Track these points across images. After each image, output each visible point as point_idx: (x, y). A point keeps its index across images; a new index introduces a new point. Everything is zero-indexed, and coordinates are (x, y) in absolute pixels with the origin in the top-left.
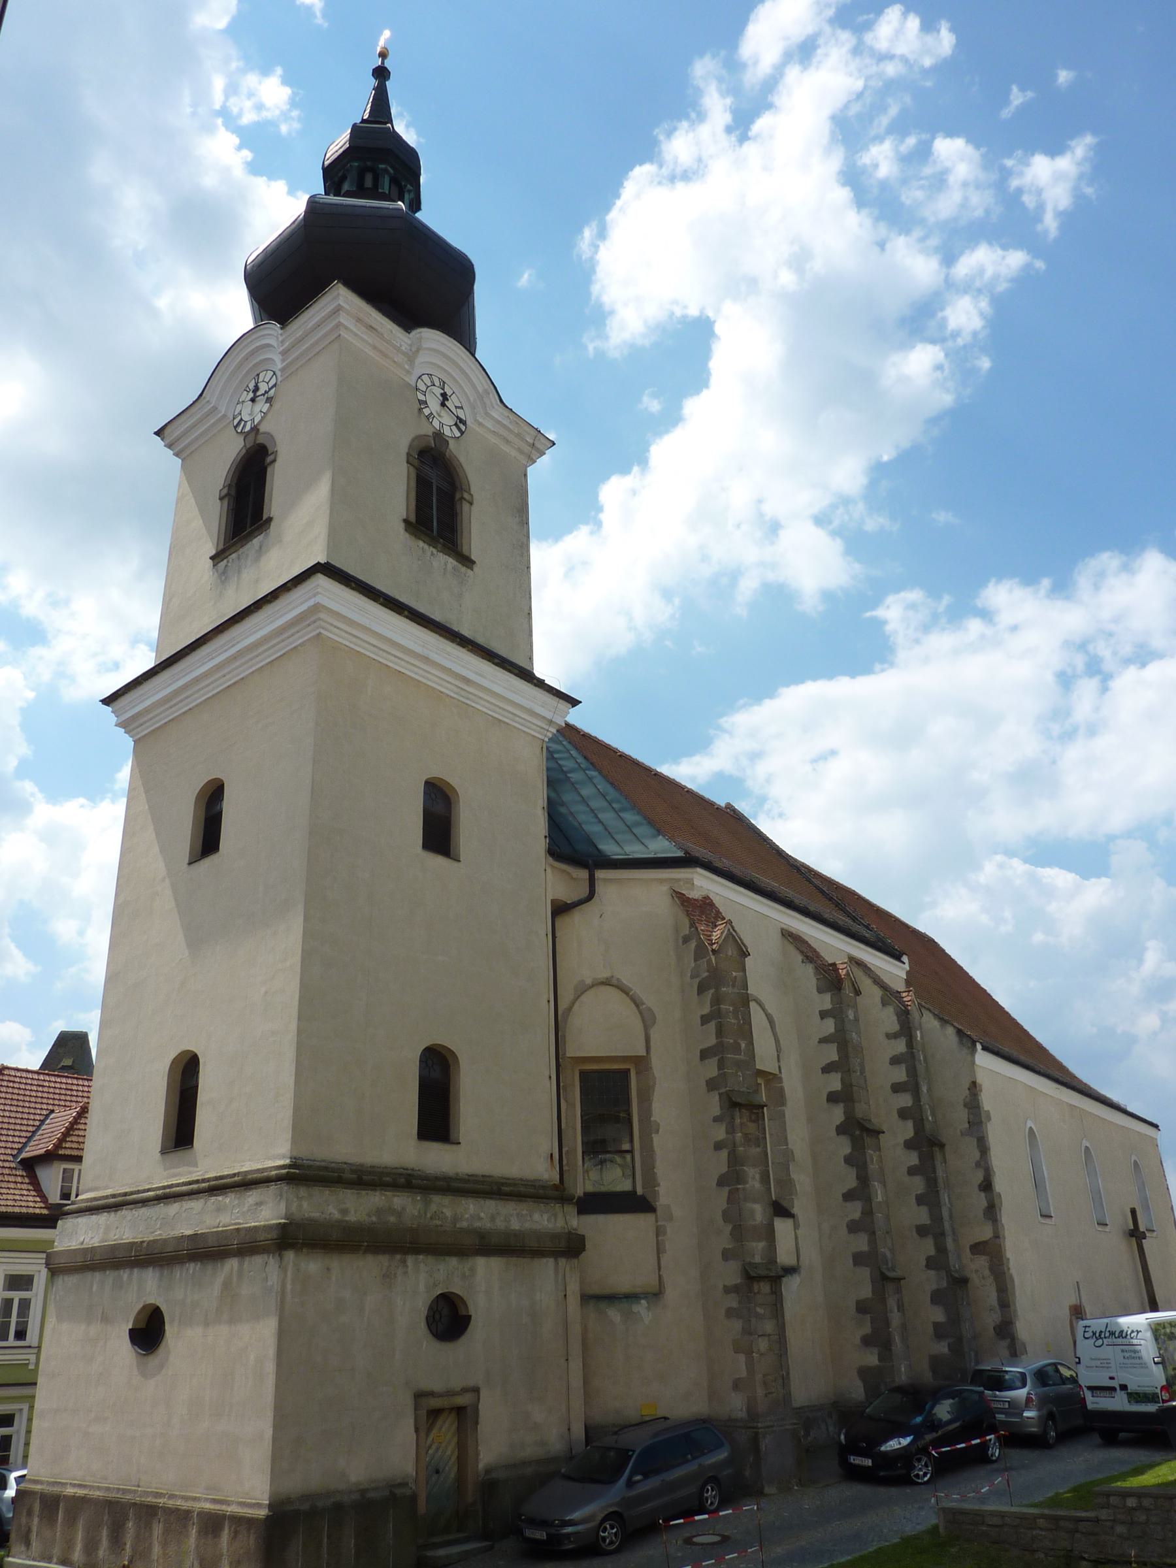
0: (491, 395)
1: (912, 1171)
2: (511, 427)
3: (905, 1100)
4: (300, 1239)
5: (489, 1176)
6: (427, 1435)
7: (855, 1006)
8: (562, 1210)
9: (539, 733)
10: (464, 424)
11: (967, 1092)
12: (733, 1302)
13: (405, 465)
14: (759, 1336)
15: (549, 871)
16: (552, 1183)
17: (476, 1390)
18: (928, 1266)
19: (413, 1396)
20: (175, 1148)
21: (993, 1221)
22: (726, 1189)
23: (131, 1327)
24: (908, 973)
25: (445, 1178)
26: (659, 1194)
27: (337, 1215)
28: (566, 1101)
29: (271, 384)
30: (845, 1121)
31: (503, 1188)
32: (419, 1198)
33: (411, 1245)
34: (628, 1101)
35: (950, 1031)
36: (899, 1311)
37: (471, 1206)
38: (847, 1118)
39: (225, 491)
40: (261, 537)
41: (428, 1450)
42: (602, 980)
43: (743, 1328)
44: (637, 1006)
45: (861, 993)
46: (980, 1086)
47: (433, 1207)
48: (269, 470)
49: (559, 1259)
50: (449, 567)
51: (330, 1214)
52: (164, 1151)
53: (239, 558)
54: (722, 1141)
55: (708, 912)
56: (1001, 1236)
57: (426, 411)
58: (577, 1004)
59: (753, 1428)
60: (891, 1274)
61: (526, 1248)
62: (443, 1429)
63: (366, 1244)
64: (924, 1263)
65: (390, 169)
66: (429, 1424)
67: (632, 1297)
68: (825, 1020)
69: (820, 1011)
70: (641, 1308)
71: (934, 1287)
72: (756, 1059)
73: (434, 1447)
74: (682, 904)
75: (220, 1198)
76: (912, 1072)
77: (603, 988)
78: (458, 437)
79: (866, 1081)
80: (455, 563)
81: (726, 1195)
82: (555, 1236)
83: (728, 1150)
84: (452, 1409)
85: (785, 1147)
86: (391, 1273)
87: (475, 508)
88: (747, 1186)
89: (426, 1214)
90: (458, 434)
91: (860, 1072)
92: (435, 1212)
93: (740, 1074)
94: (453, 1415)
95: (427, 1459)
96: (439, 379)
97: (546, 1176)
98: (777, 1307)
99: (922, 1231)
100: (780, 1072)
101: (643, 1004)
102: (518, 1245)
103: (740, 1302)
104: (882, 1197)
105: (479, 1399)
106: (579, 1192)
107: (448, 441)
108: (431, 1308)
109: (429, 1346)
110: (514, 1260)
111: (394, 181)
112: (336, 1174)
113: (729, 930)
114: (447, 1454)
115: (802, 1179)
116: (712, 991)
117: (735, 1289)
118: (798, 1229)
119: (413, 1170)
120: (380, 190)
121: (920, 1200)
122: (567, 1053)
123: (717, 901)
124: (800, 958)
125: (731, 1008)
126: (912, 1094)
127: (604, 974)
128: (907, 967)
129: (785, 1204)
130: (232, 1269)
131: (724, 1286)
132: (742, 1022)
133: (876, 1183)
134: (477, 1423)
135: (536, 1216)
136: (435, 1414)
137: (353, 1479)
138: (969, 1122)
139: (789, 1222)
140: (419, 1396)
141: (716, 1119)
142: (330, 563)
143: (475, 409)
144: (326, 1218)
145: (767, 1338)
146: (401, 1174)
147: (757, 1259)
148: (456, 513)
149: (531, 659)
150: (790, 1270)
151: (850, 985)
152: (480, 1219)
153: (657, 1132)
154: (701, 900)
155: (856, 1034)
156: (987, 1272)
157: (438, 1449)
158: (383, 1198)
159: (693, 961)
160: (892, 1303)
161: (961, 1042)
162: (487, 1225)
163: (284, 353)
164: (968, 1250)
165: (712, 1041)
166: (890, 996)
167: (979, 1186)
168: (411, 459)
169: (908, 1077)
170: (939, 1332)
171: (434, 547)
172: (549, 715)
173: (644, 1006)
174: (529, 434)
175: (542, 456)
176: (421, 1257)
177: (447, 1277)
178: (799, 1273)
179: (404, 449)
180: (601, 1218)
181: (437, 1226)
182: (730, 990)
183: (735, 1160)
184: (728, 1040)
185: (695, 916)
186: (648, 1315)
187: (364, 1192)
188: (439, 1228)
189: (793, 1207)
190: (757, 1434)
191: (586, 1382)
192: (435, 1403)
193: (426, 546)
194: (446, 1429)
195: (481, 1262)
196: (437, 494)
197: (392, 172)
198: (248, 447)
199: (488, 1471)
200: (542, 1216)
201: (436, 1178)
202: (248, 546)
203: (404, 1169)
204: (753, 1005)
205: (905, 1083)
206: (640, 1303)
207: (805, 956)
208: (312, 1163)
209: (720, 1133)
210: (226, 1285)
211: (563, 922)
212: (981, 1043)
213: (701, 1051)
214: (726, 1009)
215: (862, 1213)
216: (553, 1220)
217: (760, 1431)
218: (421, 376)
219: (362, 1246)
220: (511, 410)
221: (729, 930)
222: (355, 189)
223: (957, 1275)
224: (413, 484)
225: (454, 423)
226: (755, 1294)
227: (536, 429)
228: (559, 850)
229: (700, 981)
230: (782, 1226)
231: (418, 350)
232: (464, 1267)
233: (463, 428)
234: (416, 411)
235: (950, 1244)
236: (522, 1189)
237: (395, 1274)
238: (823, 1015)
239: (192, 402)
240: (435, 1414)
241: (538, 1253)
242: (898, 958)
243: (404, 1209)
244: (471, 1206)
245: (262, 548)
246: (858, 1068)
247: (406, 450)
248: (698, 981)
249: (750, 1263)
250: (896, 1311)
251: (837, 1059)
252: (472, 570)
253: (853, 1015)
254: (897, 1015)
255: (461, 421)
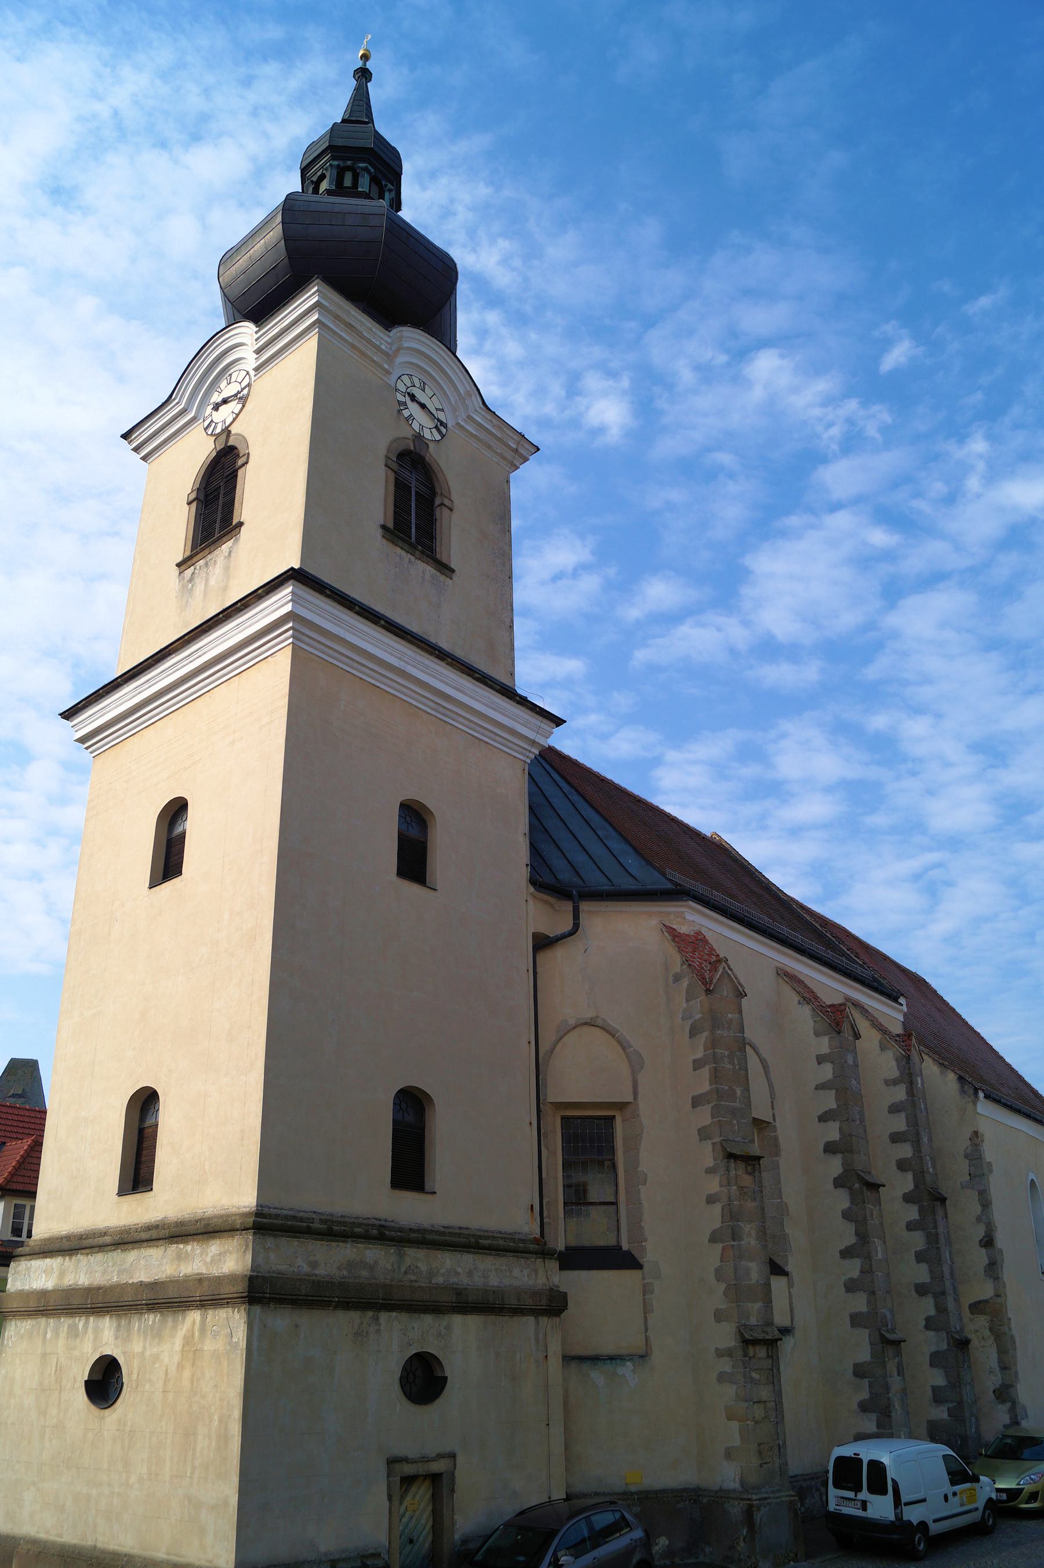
0: (473, 398)
1: (911, 1226)
2: (494, 431)
3: (905, 1151)
4: (267, 1293)
5: (466, 1228)
6: (401, 1503)
7: (854, 1051)
8: (543, 1265)
9: (521, 754)
10: (444, 427)
11: (969, 1142)
12: (725, 1365)
13: (382, 470)
14: (754, 1403)
15: (530, 902)
16: (533, 1236)
17: (453, 1456)
18: (927, 1327)
19: (386, 1463)
20: (133, 1190)
21: (994, 1279)
22: (719, 1246)
23: (86, 1379)
24: (905, 1015)
25: (420, 1230)
26: (646, 1249)
27: (306, 1269)
28: (547, 1149)
29: (244, 384)
30: (842, 1172)
31: (481, 1241)
32: (392, 1251)
33: (384, 1302)
34: (612, 1150)
35: (951, 1077)
36: (898, 1375)
37: (448, 1261)
38: (845, 1171)
39: (193, 496)
40: (230, 543)
41: (401, 1519)
42: (586, 1021)
43: (736, 1394)
44: (624, 1048)
45: (860, 1037)
46: (982, 1135)
47: (408, 1261)
48: (240, 472)
49: (540, 1318)
50: (427, 575)
51: (299, 1266)
52: (121, 1192)
53: (206, 564)
54: (715, 1194)
55: (701, 949)
56: (1003, 1295)
57: (406, 413)
58: (560, 1045)
59: (749, 1499)
60: (890, 1336)
61: (506, 1306)
62: (417, 1497)
63: (336, 1299)
64: (924, 1323)
65: (370, 168)
66: (402, 1491)
67: (617, 1359)
68: (822, 1065)
69: (817, 1055)
70: (626, 1370)
71: (933, 1349)
72: (752, 1107)
73: (408, 1515)
74: (673, 940)
75: (181, 1246)
76: (913, 1122)
77: (586, 1029)
78: (439, 441)
79: (865, 1131)
80: (434, 571)
81: (719, 1251)
82: (535, 1294)
83: (722, 1204)
84: (426, 1477)
85: (779, 1200)
86: (362, 1331)
87: (455, 516)
88: (742, 1243)
89: (399, 1269)
90: (438, 437)
91: (860, 1121)
92: (410, 1266)
93: (735, 1122)
94: (427, 1483)
95: (401, 1528)
96: (420, 379)
97: (526, 1229)
98: (773, 1372)
99: (921, 1290)
100: (774, 1119)
101: (631, 1046)
102: (497, 1302)
103: (733, 1367)
104: (882, 1255)
105: (455, 1465)
106: (561, 1247)
107: (427, 445)
108: (404, 1368)
109: (402, 1406)
110: (492, 1318)
111: (374, 180)
112: (305, 1224)
113: (724, 968)
114: (421, 1522)
115: (796, 1234)
116: (706, 1034)
117: (729, 1353)
118: (792, 1288)
119: (386, 1220)
120: (360, 189)
121: (920, 1257)
122: (548, 1099)
123: (709, 936)
124: (796, 998)
125: (726, 1053)
126: (912, 1145)
127: (588, 1014)
128: (905, 1008)
129: (779, 1261)
130: (194, 1323)
131: (716, 1348)
132: (737, 1067)
133: (876, 1240)
134: (453, 1491)
135: (516, 1272)
136: (408, 1481)
137: (323, 1548)
138: (970, 1174)
139: (783, 1280)
140: (392, 1462)
141: (709, 1171)
142: (302, 569)
143: (456, 411)
144: (294, 1271)
145: (762, 1406)
146: (374, 1225)
147: (753, 1321)
148: (436, 519)
149: (512, 674)
150: (786, 1331)
151: (850, 1028)
152: (457, 1274)
153: (645, 1183)
154: (692, 935)
155: (855, 1080)
156: (987, 1333)
157: (411, 1518)
158: (355, 1250)
159: (685, 1001)
160: (892, 1366)
161: (963, 1091)
162: (464, 1281)
163: (258, 352)
164: (967, 1310)
165: (705, 1087)
166: (890, 1040)
167: (980, 1241)
168: (390, 462)
169: (908, 1126)
170: (938, 1396)
171: (412, 554)
172: (531, 735)
173: (631, 1049)
174: (512, 438)
175: (525, 462)
176: (394, 1314)
177: (422, 1336)
178: (794, 1336)
179: (382, 451)
180: (584, 1274)
181: (411, 1281)
182: (725, 1033)
183: (732, 1216)
184: (723, 1087)
185: (687, 953)
186: (634, 1378)
187: (334, 1244)
188: (414, 1283)
189: (787, 1265)
190: (750, 1506)
191: (567, 1447)
192: (409, 1469)
193: (403, 553)
194: (420, 1497)
195: (457, 1320)
196: (416, 499)
197: (372, 170)
198: (218, 449)
199: (464, 1542)
200: (522, 1271)
201: (410, 1229)
202: (216, 552)
203: (376, 1219)
204: (748, 1047)
205: (904, 1133)
206: (625, 1365)
207: (802, 997)
208: (279, 1212)
209: (714, 1185)
210: (188, 1340)
211: (543, 957)
212: (983, 1090)
213: (693, 1098)
214: (721, 1053)
215: (861, 1272)
216: (534, 1276)
217: (754, 1503)
218: (401, 376)
219: (332, 1301)
220: (494, 413)
221: (724, 968)
222: (334, 188)
223: (957, 1337)
224: (392, 488)
225: (434, 426)
226: (750, 1358)
227: (520, 434)
228: (541, 880)
229: (692, 1023)
230: (778, 1284)
231: (398, 350)
232: (439, 1325)
233: (444, 430)
234: (396, 412)
235: (951, 1305)
236: (501, 1242)
237: (367, 1333)
238: (821, 1059)
239: (161, 404)
240: (408, 1481)
241: (518, 1311)
242: (895, 1000)
243: (376, 1262)
244: (448, 1261)
245: (232, 553)
246: (858, 1117)
247: (385, 452)
248: (690, 1023)
249: (745, 1325)
250: (896, 1373)
251: (835, 1107)
252: (451, 579)
253: (852, 1060)
254: (896, 1060)
255: (442, 423)
